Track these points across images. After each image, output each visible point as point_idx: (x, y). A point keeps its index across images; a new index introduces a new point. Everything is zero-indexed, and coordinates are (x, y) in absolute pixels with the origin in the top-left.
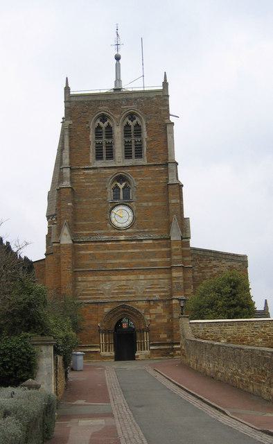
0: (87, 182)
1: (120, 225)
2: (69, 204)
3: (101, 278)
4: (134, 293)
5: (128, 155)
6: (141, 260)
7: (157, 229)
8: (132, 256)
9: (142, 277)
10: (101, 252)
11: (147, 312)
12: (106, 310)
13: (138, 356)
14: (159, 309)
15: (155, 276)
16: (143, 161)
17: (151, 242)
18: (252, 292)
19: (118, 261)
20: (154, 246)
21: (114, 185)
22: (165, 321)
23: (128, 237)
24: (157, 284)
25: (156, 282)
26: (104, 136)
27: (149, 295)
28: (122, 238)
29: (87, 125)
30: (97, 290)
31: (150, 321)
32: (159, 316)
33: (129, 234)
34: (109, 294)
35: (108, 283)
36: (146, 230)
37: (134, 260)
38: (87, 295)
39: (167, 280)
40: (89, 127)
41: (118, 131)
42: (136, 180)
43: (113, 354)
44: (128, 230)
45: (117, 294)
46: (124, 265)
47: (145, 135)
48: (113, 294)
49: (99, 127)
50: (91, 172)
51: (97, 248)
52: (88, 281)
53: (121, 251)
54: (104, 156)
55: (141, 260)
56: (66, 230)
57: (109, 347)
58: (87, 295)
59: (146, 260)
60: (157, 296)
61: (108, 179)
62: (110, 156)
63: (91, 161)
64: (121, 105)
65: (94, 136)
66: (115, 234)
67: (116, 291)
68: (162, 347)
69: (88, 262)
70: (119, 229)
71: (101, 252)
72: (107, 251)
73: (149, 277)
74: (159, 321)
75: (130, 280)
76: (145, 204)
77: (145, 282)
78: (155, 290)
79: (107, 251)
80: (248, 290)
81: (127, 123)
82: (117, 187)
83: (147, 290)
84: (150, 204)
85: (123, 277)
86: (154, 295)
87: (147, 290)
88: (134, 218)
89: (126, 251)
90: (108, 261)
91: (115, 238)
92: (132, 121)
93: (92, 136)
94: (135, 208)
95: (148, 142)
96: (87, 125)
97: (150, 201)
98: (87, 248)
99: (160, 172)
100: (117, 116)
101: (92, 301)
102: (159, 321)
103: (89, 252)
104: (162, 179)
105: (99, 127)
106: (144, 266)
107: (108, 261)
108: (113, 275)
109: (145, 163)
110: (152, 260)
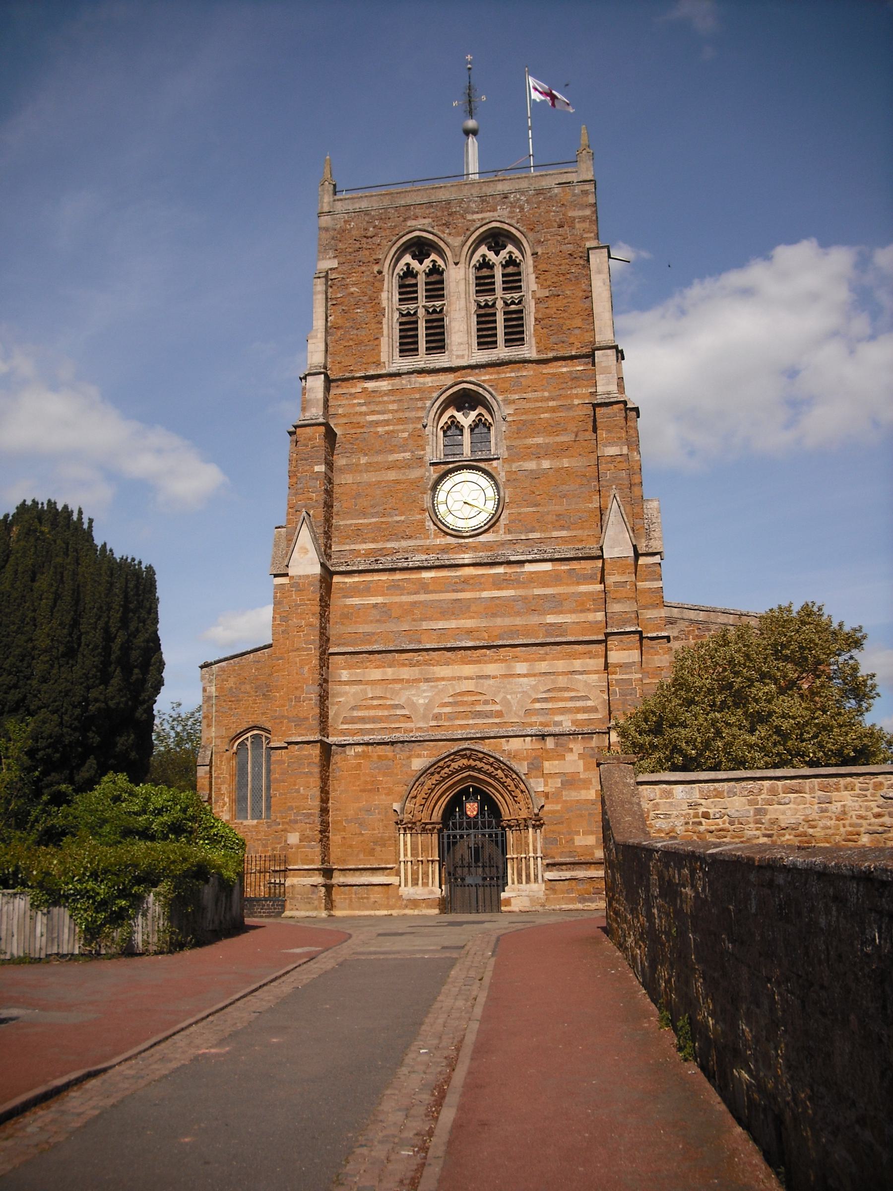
0: (373, 413)
1: (461, 524)
2: (317, 468)
3: (406, 673)
4: (499, 714)
5: (486, 340)
6: (518, 621)
7: (564, 533)
8: (494, 608)
9: (521, 668)
10: (405, 599)
11: (536, 767)
12: (418, 764)
13: (508, 902)
14: (574, 761)
15: (561, 665)
16: (529, 351)
17: (548, 566)
18: (159, 606)
19: (453, 624)
20: (554, 579)
21: (445, 418)
22: (591, 794)
23: (483, 556)
24: (567, 689)
25: (562, 681)
26: (421, 293)
27: (541, 719)
28: (467, 558)
29: (376, 268)
30: (396, 706)
31: (547, 796)
32: (570, 781)
33: (488, 546)
34: (424, 717)
35: (424, 686)
36: (536, 535)
37: (499, 621)
38: (362, 720)
39: (595, 677)
40: (380, 272)
41: (459, 280)
42: (508, 402)
43: (436, 891)
44: (482, 538)
45: (450, 717)
46: (469, 632)
47: (530, 282)
48: (437, 717)
49: (409, 273)
50: (384, 385)
51: (395, 587)
52: (367, 683)
53: (460, 595)
54: (422, 344)
55: (518, 621)
56: (305, 537)
57: (425, 874)
58: (362, 720)
59: (535, 620)
60: (566, 724)
61: (428, 403)
62: (437, 343)
63: (384, 357)
64: (467, 211)
65: (396, 297)
66: (445, 549)
67: (448, 710)
68: (580, 874)
69: (368, 628)
70: (457, 534)
71: (405, 599)
72: (422, 597)
73: (543, 666)
74: (572, 795)
75: (488, 677)
76: (531, 465)
77: (532, 681)
78: (561, 704)
79: (422, 597)
80: (156, 621)
81: (484, 256)
82: (454, 424)
83: (538, 706)
84: (546, 464)
85: (469, 670)
86: (557, 718)
87: (538, 706)
88: (500, 504)
89: (476, 595)
90: (425, 625)
91: (446, 558)
92: (497, 254)
93: (389, 296)
94: (502, 478)
95: (538, 301)
96: (376, 268)
97: (546, 455)
98: (367, 590)
99: (575, 378)
100: (456, 241)
101: (378, 738)
102: (572, 795)
103: (374, 600)
104: (580, 395)
105: (409, 273)
106: (527, 635)
107: (425, 625)
108: (438, 663)
109: (533, 355)
110: (550, 619)
